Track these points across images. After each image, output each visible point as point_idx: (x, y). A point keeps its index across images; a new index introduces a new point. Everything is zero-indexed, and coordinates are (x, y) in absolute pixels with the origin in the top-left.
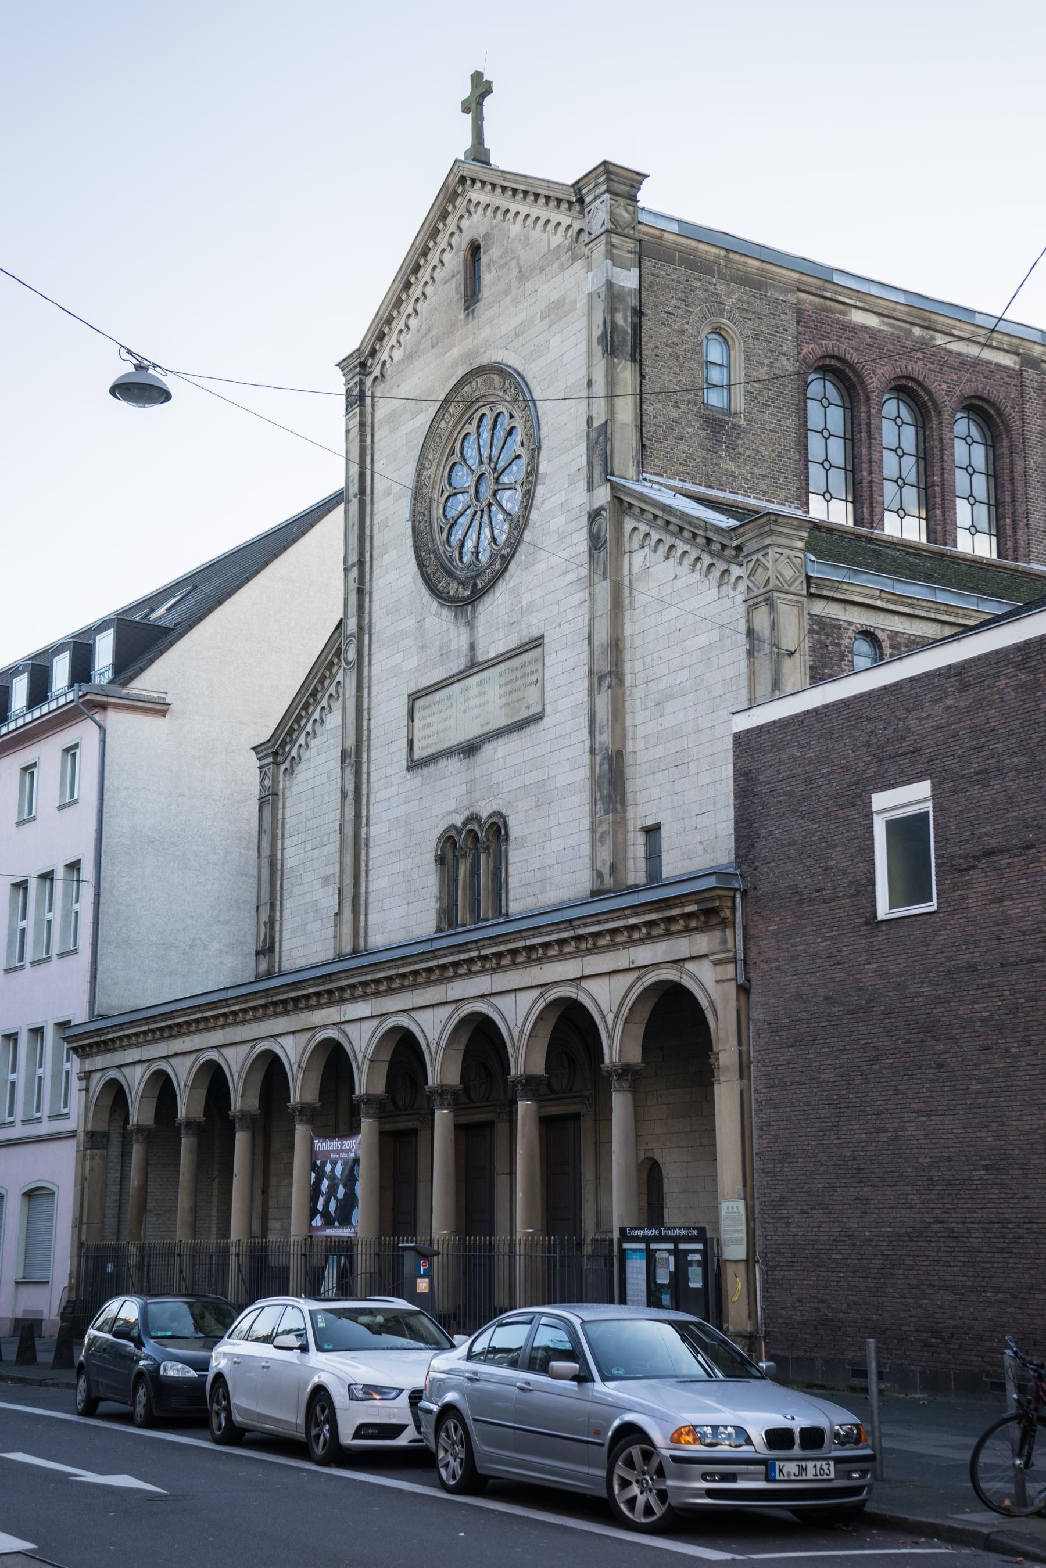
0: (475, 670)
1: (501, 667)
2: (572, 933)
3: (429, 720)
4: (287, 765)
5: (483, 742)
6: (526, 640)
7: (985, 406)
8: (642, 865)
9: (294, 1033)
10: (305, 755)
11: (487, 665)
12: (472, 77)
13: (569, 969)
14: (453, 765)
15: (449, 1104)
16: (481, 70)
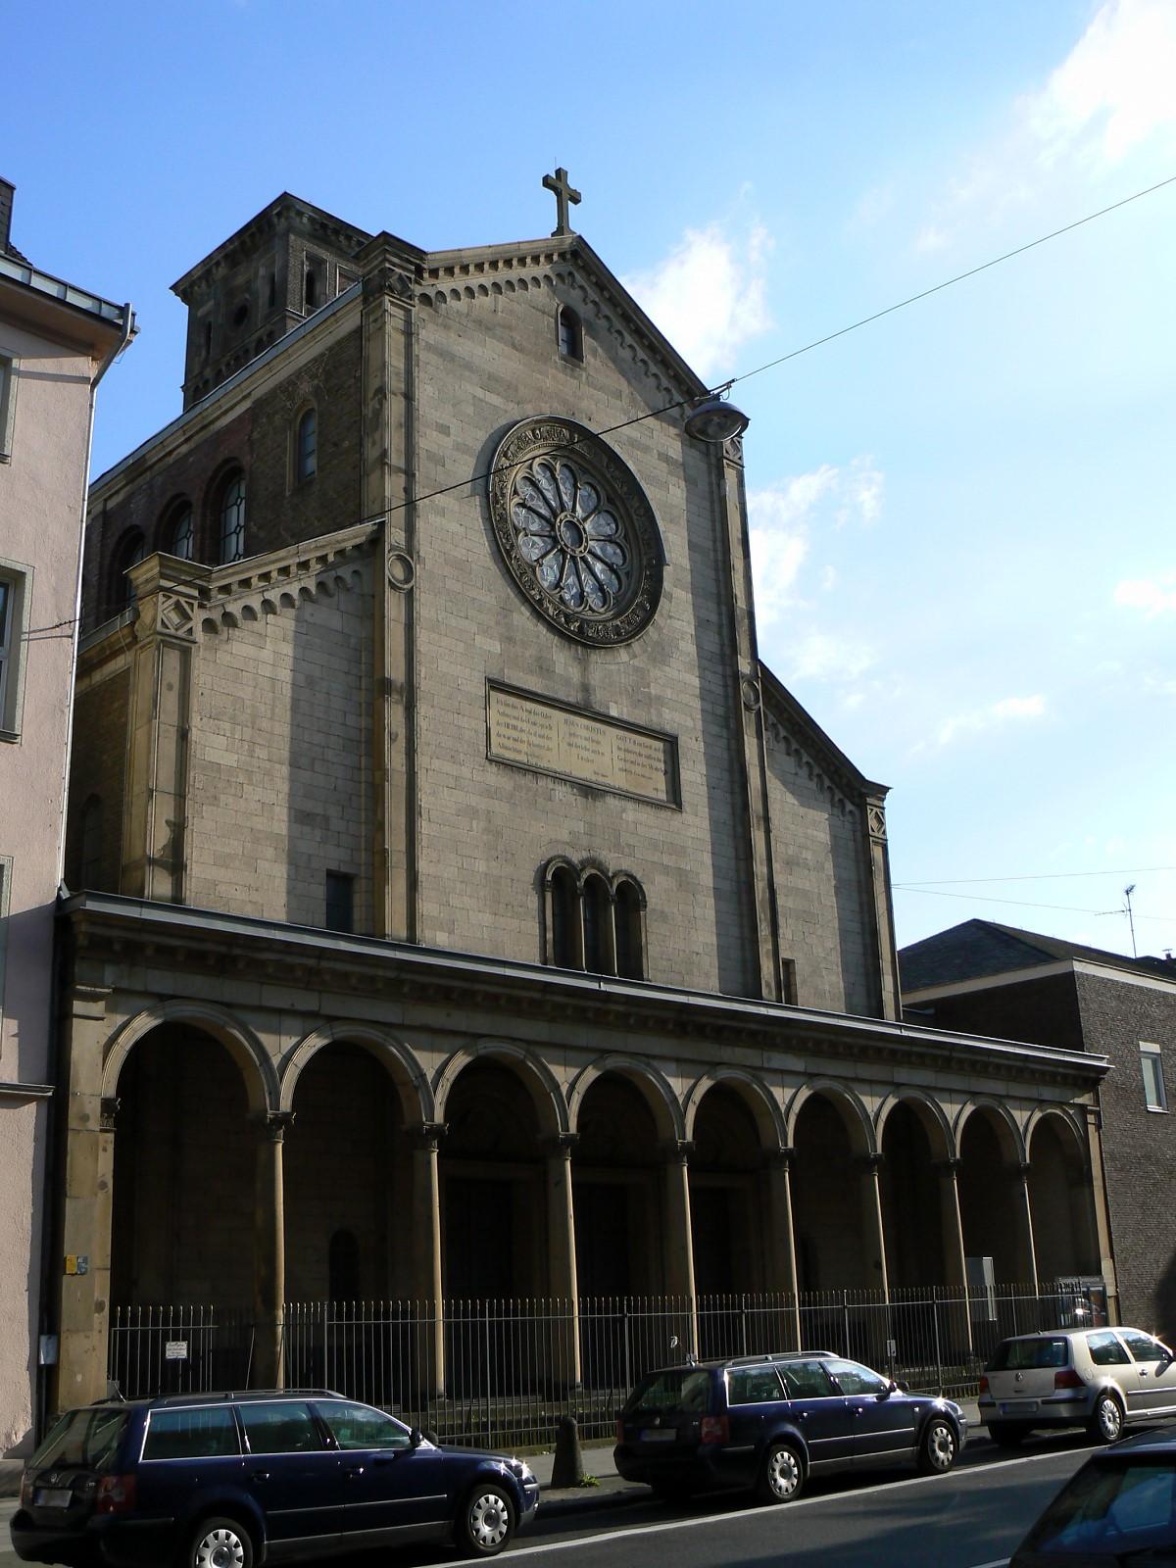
3: (519, 724)
6: (657, 728)
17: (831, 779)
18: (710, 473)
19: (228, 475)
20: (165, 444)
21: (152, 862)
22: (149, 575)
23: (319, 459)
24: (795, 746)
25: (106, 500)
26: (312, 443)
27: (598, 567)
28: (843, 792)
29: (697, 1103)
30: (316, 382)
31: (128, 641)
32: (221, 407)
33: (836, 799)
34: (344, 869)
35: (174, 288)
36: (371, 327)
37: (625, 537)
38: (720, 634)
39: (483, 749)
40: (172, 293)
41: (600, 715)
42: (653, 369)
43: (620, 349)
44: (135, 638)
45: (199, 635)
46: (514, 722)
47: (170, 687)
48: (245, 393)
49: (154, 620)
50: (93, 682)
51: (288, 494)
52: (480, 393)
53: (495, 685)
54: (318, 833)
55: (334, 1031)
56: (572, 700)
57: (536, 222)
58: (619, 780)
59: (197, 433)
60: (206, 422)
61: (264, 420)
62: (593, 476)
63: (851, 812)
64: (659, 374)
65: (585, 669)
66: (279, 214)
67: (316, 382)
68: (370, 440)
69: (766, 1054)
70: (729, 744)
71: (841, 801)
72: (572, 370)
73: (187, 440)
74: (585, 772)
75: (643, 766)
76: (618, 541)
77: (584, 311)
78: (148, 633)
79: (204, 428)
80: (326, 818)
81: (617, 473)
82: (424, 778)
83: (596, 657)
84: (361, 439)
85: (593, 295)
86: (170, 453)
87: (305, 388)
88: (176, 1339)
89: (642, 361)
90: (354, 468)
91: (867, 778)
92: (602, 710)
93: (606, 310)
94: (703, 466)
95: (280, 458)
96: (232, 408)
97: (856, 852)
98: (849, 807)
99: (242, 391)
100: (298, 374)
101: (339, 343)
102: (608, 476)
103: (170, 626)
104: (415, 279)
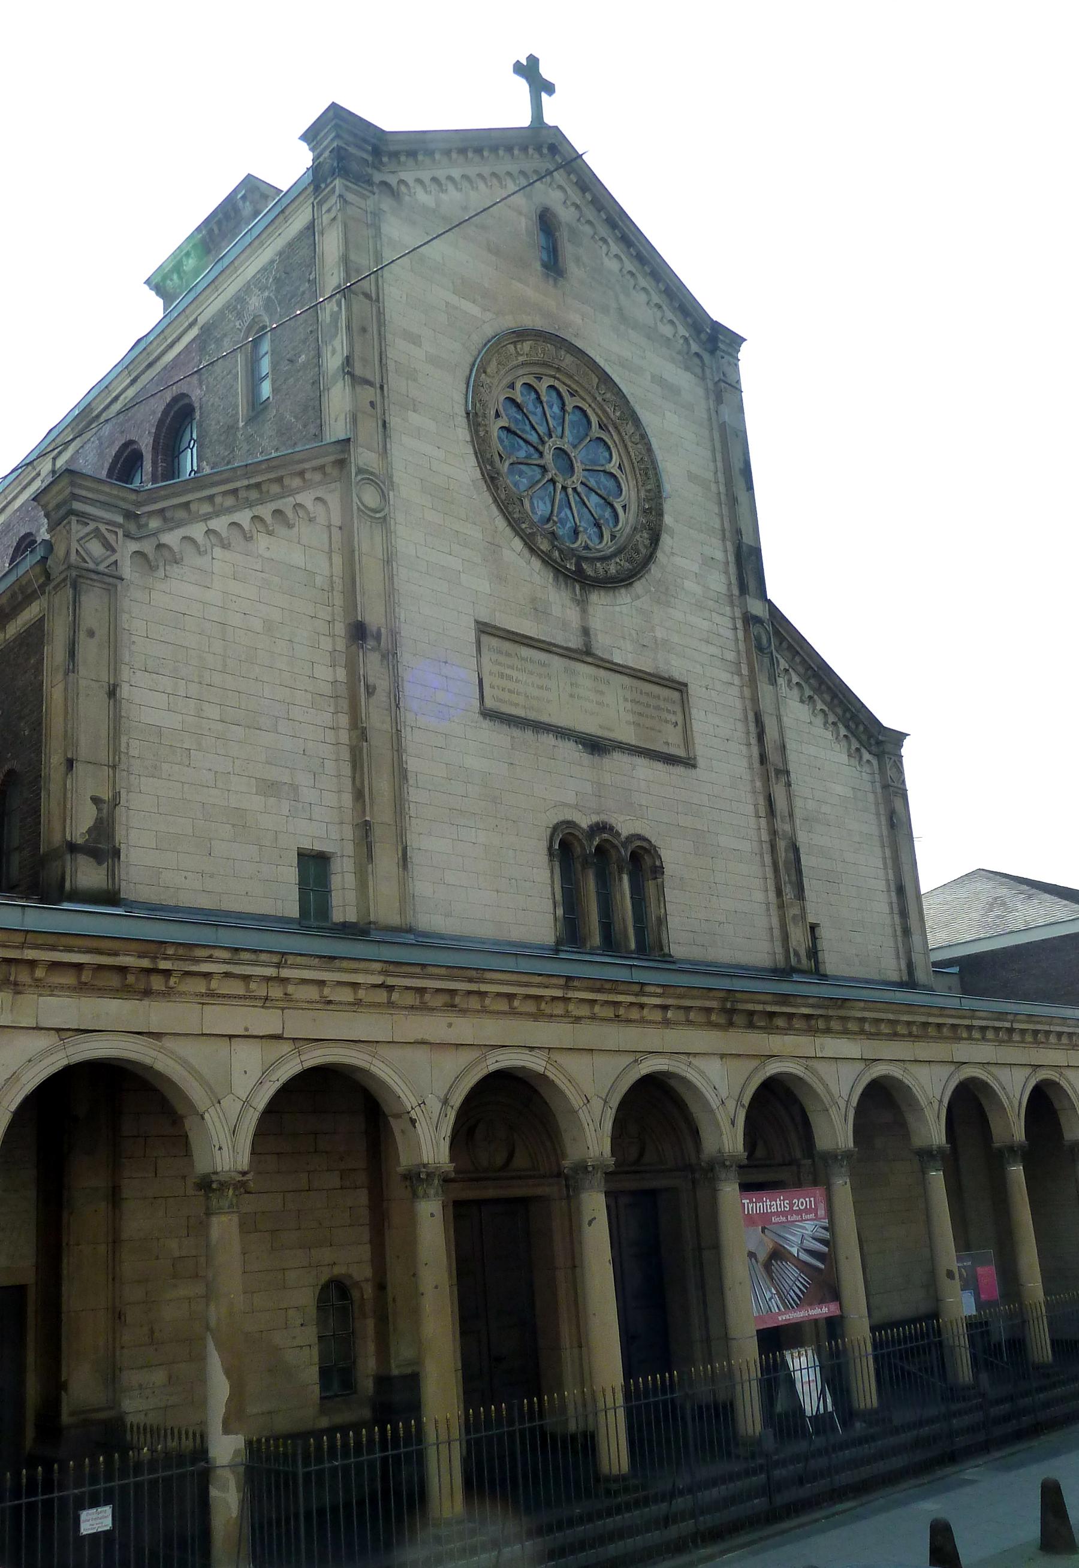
0: (590, 660)
1: (627, 681)
2: (733, 1001)
3: (515, 674)
4: (147, 547)
5: (614, 748)
7: (176, 408)
8: (351, 896)
9: (722, 1056)
10: (192, 559)
11: (607, 665)
12: (514, 65)
13: (984, 1052)
14: (570, 750)
15: (436, 1194)
16: (554, 96)
17: (847, 727)
18: (708, 399)
19: (178, 418)
20: (110, 388)
21: (73, 848)
22: (60, 498)
23: (273, 382)
24: (808, 692)
25: (54, 459)
26: (265, 366)
27: (593, 501)
28: (860, 742)
29: (747, 1105)
30: (266, 294)
31: (41, 581)
32: (166, 339)
33: (853, 748)
34: (318, 847)
35: (148, 282)
36: (324, 217)
37: (620, 467)
38: (726, 572)
39: (477, 703)
40: (146, 287)
41: (602, 660)
42: (643, 282)
43: (606, 260)
44: (48, 577)
45: (127, 570)
46: (508, 672)
47: (91, 634)
48: (191, 319)
49: (68, 553)
50: (7, 637)
51: (241, 424)
52: (454, 300)
53: (484, 629)
54: (285, 806)
55: (303, 1058)
56: (571, 645)
57: (511, 110)
58: (627, 734)
59: (143, 372)
60: (151, 359)
61: (213, 346)
62: (584, 399)
63: (868, 761)
64: (648, 287)
65: (584, 611)
66: (244, 197)
67: (266, 294)
68: (330, 348)
69: (818, 1041)
70: (742, 692)
71: (858, 750)
72: (555, 280)
73: (134, 381)
74: (590, 726)
75: (652, 717)
76: (612, 471)
77: (565, 215)
78: (62, 568)
79: (150, 365)
80: (294, 788)
81: (608, 395)
82: (409, 738)
83: (598, 599)
84: (318, 349)
85: (575, 196)
86: (116, 398)
87: (255, 302)
88: (95, 1503)
89: (630, 272)
90: (313, 383)
91: (886, 724)
92: (606, 656)
93: (590, 213)
94: (700, 392)
95: (232, 387)
96: (179, 338)
97: (877, 804)
98: (866, 756)
99: (187, 317)
100: (247, 289)
101: (290, 245)
102: (599, 399)
103: (87, 559)
104: (373, 163)
